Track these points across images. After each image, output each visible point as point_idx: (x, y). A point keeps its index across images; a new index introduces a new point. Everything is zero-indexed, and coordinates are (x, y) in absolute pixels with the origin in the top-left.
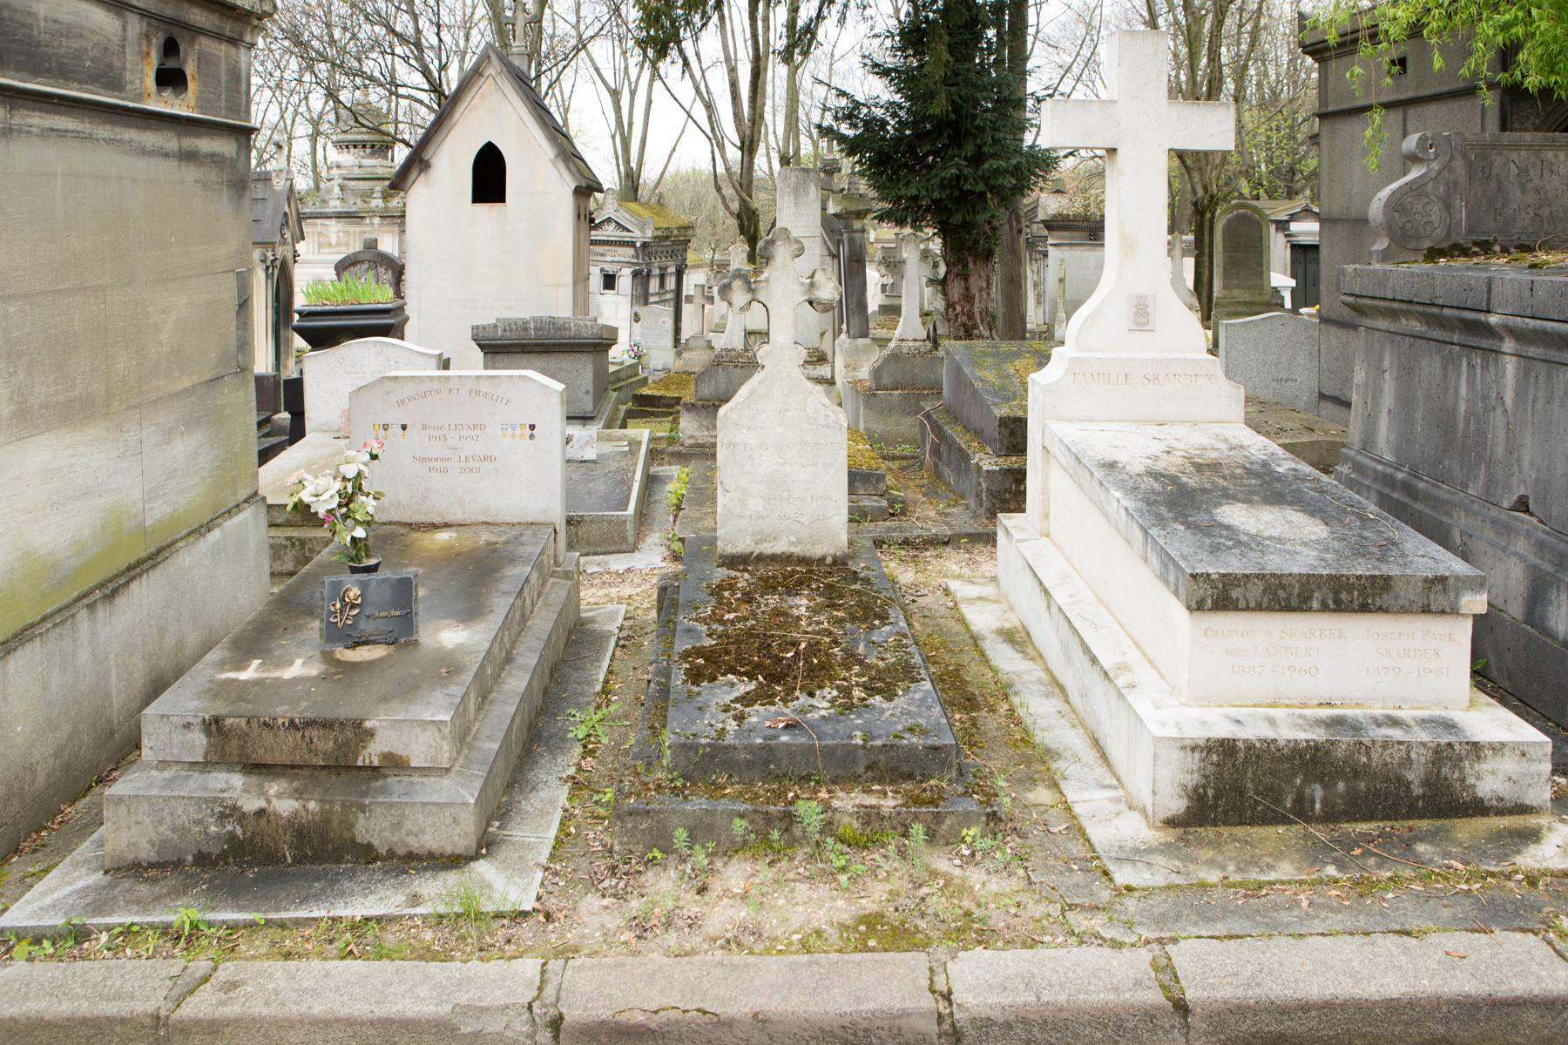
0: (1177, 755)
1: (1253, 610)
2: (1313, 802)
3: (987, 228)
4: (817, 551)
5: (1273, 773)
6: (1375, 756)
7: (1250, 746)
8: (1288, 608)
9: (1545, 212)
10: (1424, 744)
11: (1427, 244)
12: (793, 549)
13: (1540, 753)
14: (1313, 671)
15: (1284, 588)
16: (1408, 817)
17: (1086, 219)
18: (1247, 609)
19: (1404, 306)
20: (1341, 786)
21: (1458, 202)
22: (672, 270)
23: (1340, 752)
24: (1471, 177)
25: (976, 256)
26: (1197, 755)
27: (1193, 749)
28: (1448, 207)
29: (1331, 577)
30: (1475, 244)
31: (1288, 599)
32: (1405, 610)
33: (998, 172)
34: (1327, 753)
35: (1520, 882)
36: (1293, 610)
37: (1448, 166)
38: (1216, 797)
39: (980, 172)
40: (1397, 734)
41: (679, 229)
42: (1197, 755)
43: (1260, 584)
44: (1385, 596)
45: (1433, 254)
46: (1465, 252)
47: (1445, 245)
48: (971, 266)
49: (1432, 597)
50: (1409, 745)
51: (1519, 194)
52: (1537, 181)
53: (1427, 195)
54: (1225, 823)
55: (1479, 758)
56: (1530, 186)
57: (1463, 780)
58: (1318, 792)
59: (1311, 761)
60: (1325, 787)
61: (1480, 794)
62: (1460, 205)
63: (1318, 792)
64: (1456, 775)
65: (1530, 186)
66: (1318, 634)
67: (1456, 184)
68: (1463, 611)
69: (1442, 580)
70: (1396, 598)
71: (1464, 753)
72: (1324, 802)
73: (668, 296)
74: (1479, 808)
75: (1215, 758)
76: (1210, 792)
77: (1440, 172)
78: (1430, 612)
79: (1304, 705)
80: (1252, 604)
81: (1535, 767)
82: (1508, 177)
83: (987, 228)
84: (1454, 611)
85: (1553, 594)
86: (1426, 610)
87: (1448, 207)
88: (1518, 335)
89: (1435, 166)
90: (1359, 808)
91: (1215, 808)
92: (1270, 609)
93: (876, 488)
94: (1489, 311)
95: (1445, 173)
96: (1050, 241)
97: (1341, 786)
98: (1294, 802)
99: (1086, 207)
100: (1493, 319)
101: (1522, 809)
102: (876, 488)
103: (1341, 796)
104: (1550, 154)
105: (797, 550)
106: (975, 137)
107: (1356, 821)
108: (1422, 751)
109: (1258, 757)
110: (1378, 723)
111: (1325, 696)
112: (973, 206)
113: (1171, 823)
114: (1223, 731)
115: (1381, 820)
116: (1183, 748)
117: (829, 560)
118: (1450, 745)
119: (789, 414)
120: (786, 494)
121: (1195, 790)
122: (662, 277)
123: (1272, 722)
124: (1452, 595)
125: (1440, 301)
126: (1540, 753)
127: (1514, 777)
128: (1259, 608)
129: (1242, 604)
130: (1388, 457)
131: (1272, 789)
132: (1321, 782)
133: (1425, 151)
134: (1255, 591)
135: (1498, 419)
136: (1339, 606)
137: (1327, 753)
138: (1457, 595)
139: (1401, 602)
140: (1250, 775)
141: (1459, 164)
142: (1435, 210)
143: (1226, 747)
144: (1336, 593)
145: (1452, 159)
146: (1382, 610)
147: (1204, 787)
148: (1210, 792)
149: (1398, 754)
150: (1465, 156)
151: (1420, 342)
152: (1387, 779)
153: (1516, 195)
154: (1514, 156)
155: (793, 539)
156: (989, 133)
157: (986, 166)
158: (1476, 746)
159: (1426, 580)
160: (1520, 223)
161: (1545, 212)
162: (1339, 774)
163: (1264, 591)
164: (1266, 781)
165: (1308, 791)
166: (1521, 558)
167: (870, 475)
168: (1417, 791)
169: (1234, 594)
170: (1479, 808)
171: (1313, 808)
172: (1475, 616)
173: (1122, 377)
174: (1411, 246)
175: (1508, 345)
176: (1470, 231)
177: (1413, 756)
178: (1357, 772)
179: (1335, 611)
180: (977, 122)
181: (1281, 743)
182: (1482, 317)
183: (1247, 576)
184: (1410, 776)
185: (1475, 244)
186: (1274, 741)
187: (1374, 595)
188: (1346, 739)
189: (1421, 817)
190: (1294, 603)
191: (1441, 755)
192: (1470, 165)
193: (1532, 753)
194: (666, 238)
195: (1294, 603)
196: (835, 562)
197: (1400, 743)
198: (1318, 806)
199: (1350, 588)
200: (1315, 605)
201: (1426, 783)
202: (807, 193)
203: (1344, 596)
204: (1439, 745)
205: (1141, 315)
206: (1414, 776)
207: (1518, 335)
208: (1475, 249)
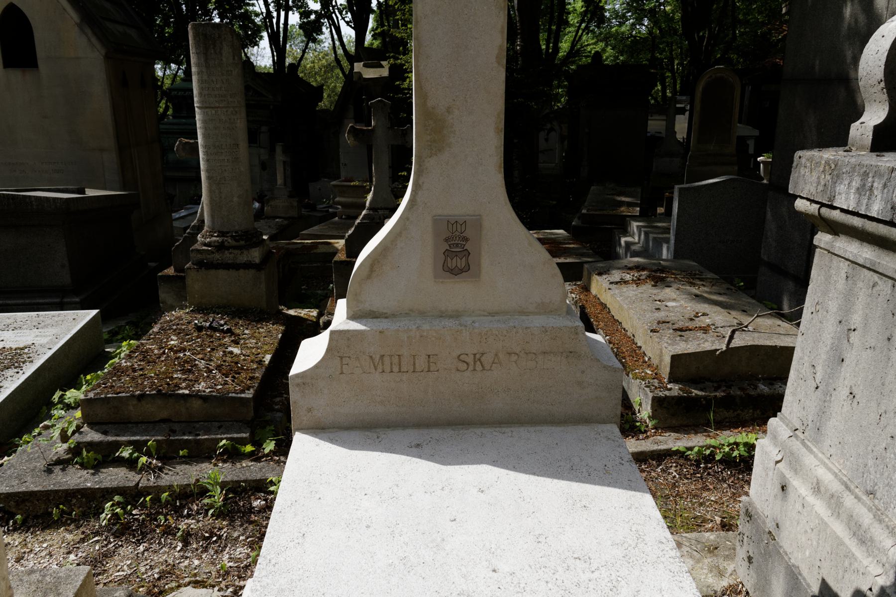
173: (421, 363)
205: (457, 251)
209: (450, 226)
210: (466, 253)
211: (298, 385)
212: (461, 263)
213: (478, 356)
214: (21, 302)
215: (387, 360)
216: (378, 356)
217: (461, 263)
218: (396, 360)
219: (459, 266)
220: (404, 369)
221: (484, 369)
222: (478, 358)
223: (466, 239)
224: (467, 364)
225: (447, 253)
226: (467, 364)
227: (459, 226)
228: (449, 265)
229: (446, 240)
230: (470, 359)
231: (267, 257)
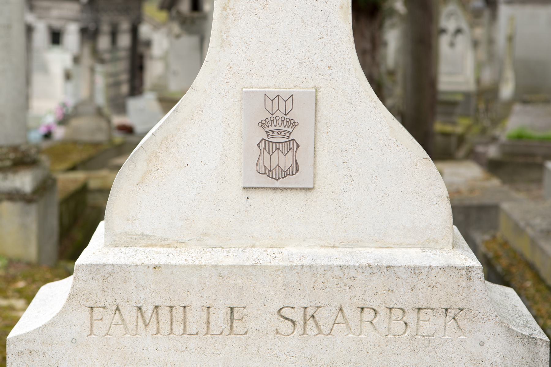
111: (279, 196)
173: (220, 317)
205: (279, 145)
209: (269, 102)
210: (293, 144)
211: (20, 353)
212: (286, 161)
213: (310, 312)
214: (304, 90)
215: (164, 313)
216: (151, 308)
217: (286, 161)
218: (178, 313)
219: (282, 165)
220: (192, 329)
221: (320, 332)
222: (310, 317)
223: (294, 124)
224: (294, 323)
225: (263, 145)
226: (294, 323)
227: (282, 103)
228: (267, 164)
229: (262, 124)
230: (298, 316)
231: (44, 187)
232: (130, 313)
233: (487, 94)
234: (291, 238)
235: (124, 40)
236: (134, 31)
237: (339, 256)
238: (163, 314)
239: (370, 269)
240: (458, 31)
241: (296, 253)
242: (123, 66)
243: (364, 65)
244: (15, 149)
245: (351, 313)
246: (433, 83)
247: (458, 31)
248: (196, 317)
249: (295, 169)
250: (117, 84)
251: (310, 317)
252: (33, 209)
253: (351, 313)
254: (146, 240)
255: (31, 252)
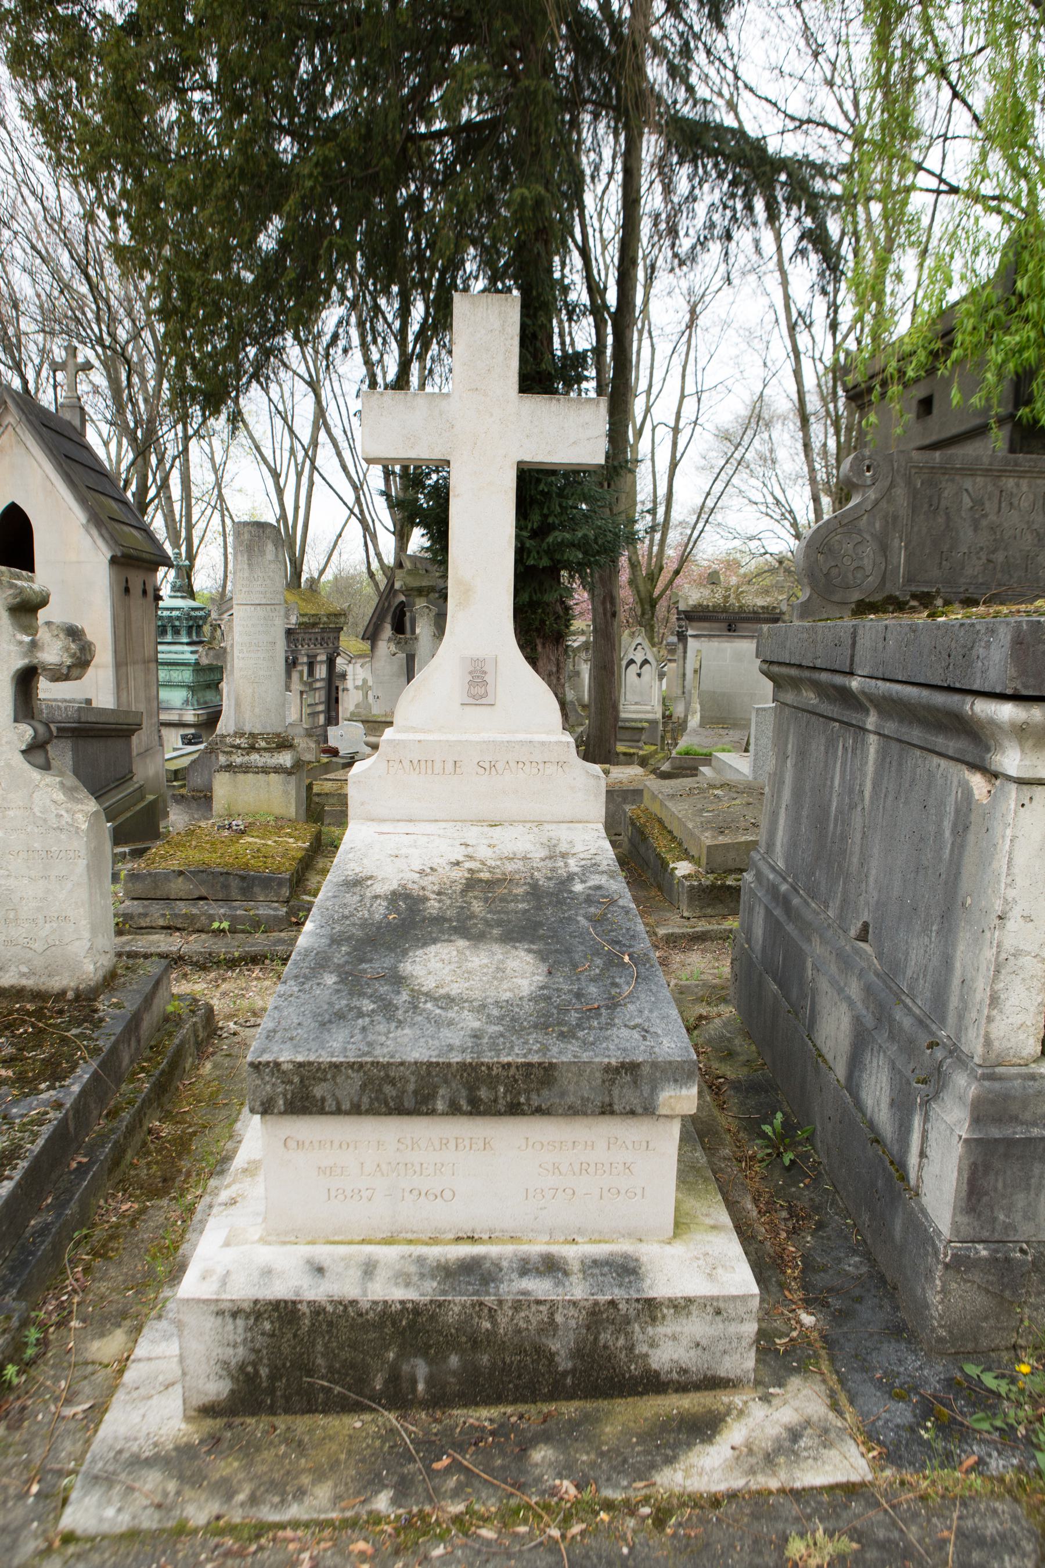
0: (210, 1323)
1: (348, 1113)
2: (414, 1382)
3: (559, 609)
4: (55, 984)
5: (354, 1346)
6: (502, 1320)
7: (317, 1310)
8: (399, 1110)
9: (1000, 557)
10: (575, 1304)
11: (856, 596)
12: (24, 982)
13: (741, 1310)
14: (448, 1194)
15: (393, 1082)
16: (551, 1397)
17: (725, 610)
18: (339, 1111)
19: (793, 672)
20: (454, 1360)
21: (896, 541)
22: (322, 657)
23: (452, 1316)
24: (914, 509)
25: (545, 638)
26: (240, 1322)
27: (235, 1315)
28: (884, 548)
29: (463, 1066)
30: (914, 596)
31: (399, 1098)
32: (574, 1112)
33: (562, 545)
34: (433, 1317)
35: (644, 1518)
36: (409, 1113)
37: (887, 494)
38: (273, 1377)
39: (544, 546)
40: (540, 1287)
41: (328, 616)
42: (240, 1322)
43: (357, 1079)
44: (545, 1092)
45: (863, 608)
46: (900, 606)
47: (878, 597)
48: (540, 648)
49: (616, 1092)
50: (553, 1306)
51: (970, 533)
52: (992, 517)
53: (859, 532)
54: (288, 1410)
55: (654, 1319)
56: (984, 523)
57: (631, 1348)
58: (421, 1369)
59: (408, 1328)
60: (430, 1362)
61: (655, 1366)
62: (897, 544)
63: (421, 1369)
64: (621, 1342)
65: (984, 523)
66: (452, 1145)
67: (895, 518)
68: (663, 1111)
69: (631, 1068)
70: (563, 1094)
71: (632, 1313)
72: (430, 1381)
73: (318, 685)
74: (653, 1384)
75: (267, 1326)
76: (264, 1372)
77: (877, 502)
78: (612, 1113)
79: (434, 1241)
80: (346, 1106)
81: (733, 1329)
82: (959, 510)
83: (559, 609)
84: (648, 1110)
85: (868, 1057)
86: (607, 1110)
87: (884, 548)
88: (889, 707)
89: (872, 494)
90: (478, 1389)
91: (271, 1391)
92: (372, 1111)
93: (278, 894)
94: (852, 674)
95: (884, 504)
96: (690, 632)
97: (454, 1360)
98: (386, 1382)
99: (726, 598)
100: (855, 684)
101: (714, 1383)
102: (278, 894)
103: (454, 1373)
104: (1010, 483)
105: (28, 983)
106: (541, 505)
107: (477, 1404)
108: (572, 1312)
109: (330, 1324)
110: (525, 1267)
111: (466, 1227)
112: (541, 584)
113: (208, 1411)
114: (279, 1290)
115: (514, 1402)
116: (220, 1313)
117: (70, 995)
118: (612, 1303)
119: (11, 813)
120: (12, 915)
121: (242, 1367)
122: (311, 666)
123: (369, 1269)
124: (646, 1090)
125: (819, 663)
126: (741, 1310)
127: (704, 1342)
128: (356, 1110)
129: (330, 1104)
130: (781, 864)
131: (353, 1366)
132: (425, 1355)
133: (860, 474)
134: (349, 1088)
135: (857, 820)
136: (477, 1108)
137: (433, 1317)
138: (654, 1090)
139: (570, 1099)
140: (319, 1348)
141: (900, 492)
142: (869, 553)
143: (284, 1312)
144: (472, 1089)
145: (892, 485)
146: (539, 1111)
147: (254, 1364)
148: (264, 1372)
149: (536, 1317)
150: (909, 482)
151: (814, 718)
152: (520, 1350)
153: (967, 535)
154: (968, 483)
155: (24, 969)
156: (556, 501)
157: (550, 539)
158: (651, 1305)
159: (608, 1069)
160: (969, 571)
161: (1000, 557)
162: (451, 1344)
163: (363, 1087)
164: (345, 1354)
165: (405, 1368)
166: (851, 1004)
167: (270, 879)
168: (564, 1364)
169: (318, 1091)
170: (653, 1384)
171: (414, 1389)
172: (683, 1118)
173: (449, 766)
174: (836, 598)
175: (871, 721)
176: (910, 580)
177: (559, 1319)
178: (476, 1343)
179: (470, 1114)
180: (541, 487)
181: (364, 1306)
182: (839, 680)
183: (336, 1066)
184: (554, 1345)
185: (914, 596)
186: (354, 1303)
187: (528, 1092)
188: (459, 1300)
189: (570, 1397)
190: (409, 1103)
191: (598, 1316)
192: (914, 495)
193: (731, 1310)
194: (314, 625)
195: (409, 1103)
196: (78, 997)
197: (539, 1302)
198: (421, 1387)
199: (492, 1081)
200: (440, 1105)
201: (578, 1354)
202: (262, 553)
203: (483, 1093)
204: (596, 1303)
205: (478, 684)
206: (560, 1346)
207: (889, 707)
208: (913, 603)
232: (406, 763)
233: (672, 725)
234: (482, 728)
235: (321, 671)
236: (331, 663)
237: (506, 737)
238: (422, 764)
239: (521, 743)
240: (646, 662)
241: (485, 736)
242: (320, 696)
243: (522, 647)
244: (278, 735)
245: (513, 764)
246: (615, 707)
247: (646, 662)
248: (438, 766)
249: (486, 695)
250: (314, 715)
251: (493, 766)
252: (293, 779)
253: (513, 764)
254: (414, 729)
255: (292, 812)
